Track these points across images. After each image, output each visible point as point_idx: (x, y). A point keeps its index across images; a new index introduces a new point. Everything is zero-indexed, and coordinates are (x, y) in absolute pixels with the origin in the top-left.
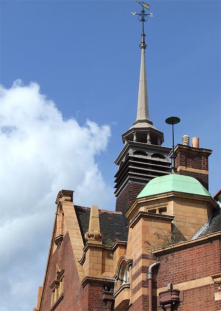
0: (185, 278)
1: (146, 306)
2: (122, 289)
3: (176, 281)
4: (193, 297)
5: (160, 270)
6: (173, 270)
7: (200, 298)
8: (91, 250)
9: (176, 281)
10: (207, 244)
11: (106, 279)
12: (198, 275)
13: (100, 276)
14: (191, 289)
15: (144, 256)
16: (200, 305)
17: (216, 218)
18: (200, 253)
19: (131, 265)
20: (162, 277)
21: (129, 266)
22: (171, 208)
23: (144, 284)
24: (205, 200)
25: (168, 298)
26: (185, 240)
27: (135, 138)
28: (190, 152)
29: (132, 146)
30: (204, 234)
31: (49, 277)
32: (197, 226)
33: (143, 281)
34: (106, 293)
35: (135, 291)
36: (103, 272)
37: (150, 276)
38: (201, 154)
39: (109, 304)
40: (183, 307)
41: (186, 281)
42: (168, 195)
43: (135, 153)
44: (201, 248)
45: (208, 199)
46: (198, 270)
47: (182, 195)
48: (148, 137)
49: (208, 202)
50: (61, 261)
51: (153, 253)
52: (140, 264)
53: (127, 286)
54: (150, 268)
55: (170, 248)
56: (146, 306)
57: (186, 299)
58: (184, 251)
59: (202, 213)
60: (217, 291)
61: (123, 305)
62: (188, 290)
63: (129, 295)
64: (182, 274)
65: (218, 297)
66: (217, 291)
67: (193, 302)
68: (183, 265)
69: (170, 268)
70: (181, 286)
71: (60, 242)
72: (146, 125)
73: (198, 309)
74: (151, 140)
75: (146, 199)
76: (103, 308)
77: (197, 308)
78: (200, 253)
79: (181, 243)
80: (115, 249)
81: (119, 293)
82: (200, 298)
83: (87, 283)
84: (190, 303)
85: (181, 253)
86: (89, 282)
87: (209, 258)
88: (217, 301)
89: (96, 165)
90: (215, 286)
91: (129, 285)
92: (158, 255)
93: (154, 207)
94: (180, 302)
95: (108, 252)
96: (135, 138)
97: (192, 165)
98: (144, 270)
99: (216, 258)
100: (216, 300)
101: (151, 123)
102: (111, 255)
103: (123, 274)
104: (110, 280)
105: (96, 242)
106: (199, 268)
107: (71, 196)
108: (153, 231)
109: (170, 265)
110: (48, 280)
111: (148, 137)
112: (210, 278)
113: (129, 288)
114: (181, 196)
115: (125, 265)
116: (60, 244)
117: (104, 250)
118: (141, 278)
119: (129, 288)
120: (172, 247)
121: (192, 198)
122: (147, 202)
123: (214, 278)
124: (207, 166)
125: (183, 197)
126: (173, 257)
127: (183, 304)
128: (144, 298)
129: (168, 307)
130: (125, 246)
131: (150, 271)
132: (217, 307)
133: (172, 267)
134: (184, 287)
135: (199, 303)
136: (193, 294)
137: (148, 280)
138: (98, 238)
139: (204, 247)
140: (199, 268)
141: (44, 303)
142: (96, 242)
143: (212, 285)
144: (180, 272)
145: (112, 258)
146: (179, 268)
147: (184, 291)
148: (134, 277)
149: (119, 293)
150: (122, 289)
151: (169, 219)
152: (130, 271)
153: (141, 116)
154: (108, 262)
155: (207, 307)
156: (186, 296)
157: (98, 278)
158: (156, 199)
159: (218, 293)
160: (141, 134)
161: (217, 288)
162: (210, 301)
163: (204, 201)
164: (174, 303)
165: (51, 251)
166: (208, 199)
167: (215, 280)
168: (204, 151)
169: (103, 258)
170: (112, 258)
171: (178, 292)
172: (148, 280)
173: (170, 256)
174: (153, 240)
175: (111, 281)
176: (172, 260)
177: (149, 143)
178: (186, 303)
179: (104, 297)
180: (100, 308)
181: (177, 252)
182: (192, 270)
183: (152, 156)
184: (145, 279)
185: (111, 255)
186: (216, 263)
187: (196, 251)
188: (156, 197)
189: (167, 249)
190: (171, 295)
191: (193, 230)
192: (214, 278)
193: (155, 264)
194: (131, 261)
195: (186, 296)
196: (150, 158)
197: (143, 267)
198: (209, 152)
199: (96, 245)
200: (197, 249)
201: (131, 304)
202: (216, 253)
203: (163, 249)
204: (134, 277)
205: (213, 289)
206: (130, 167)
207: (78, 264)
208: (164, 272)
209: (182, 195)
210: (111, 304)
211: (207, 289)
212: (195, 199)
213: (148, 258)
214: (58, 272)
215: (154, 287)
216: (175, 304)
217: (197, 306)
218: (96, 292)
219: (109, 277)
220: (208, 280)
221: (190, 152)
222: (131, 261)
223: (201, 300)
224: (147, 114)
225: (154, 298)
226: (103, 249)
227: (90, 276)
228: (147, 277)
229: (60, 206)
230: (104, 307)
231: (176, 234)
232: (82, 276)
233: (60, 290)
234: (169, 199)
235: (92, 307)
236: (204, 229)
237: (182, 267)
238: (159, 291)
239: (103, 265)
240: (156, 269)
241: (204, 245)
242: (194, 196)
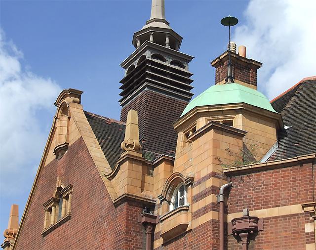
0: (266, 204)
1: (216, 233)
2: (178, 212)
3: (254, 206)
4: (276, 226)
5: (232, 192)
6: (249, 194)
7: (286, 228)
8: (130, 162)
9: (254, 206)
10: (296, 167)
11: (146, 199)
12: (283, 202)
13: (138, 194)
14: (274, 218)
15: (214, 175)
16: (286, 237)
17: (284, 140)
18: (286, 176)
19: (191, 184)
20: (235, 201)
21: (189, 185)
22: (239, 122)
23: (214, 207)
24: (275, 118)
25: (246, 225)
26: (253, 159)
27: (151, 39)
28: (239, 62)
29: (150, 47)
30: (272, 158)
31: (38, 193)
32: (267, 147)
33: (213, 203)
34: (147, 216)
35: (196, 215)
36: (142, 190)
37: (221, 199)
38: (249, 66)
39: (149, 228)
40: (262, 237)
41: (267, 208)
42: (236, 107)
43: (153, 57)
44: (287, 170)
45: (278, 117)
46: (283, 196)
47: (251, 109)
48: (167, 40)
49: (278, 120)
50: (66, 174)
51: (224, 171)
52: (210, 183)
53: (185, 208)
54: (222, 189)
55: (247, 168)
56: (216, 233)
57: (266, 228)
58: (265, 172)
59: (271, 132)
60: (308, 222)
61: (176, 231)
62: (270, 218)
63: (187, 219)
64: (262, 200)
65: (309, 228)
66: (308, 221)
67: (276, 233)
68: (263, 188)
69: (246, 191)
70: (261, 213)
71: (63, 151)
72: (164, 26)
73: (283, 240)
74: (170, 44)
75: (208, 109)
76: (142, 233)
77: (281, 239)
78: (286, 176)
79: (252, 165)
80: (157, 164)
81: (169, 217)
82: (286, 228)
83: (125, 201)
84: (272, 233)
85: (261, 174)
86: (128, 200)
87: (298, 183)
88: (308, 233)
89: (30, 74)
90: (306, 216)
91: (188, 207)
92: (229, 175)
93: (217, 119)
94: (258, 231)
95: (149, 167)
96: (151, 39)
97: (240, 78)
98: (214, 190)
99: (308, 184)
100: (307, 231)
101: (168, 24)
102: (151, 171)
103: (171, 194)
104: (151, 200)
105: (136, 154)
106: (284, 194)
107: (79, 97)
108: (224, 146)
109: (245, 188)
110: (36, 196)
111: (167, 40)
112: (300, 206)
113: (187, 210)
114: (251, 110)
115: (178, 184)
116: (63, 154)
117: (144, 165)
118: (210, 199)
119: (187, 210)
120: (250, 167)
121: (262, 114)
122: (209, 111)
123: (304, 207)
124: (256, 80)
125: (253, 111)
126: (250, 179)
127: (262, 234)
128: (214, 223)
129: (244, 236)
130: (171, 162)
131: (221, 191)
132: (308, 240)
133: (248, 190)
134: (263, 214)
135: (284, 234)
136: (277, 224)
137: (219, 203)
138: (138, 149)
139: (291, 170)
140: (284, 194)
141: (26, 224)
142: (136, 154)
143: (301, 214)
144: (259, 197)
145: (151, 174)
146: (257, 192)
147: (265, 219)
148: (196, 199)
149: (169, 217)
150: (178, 212)
151: (239, 134)
152: (189, 191)
153: (156, 13)
154: (148, 178)
155: (294, 239)
156: (267, 225)
157: (137, 197)
158: (221, 109)
159: (309, 224)
160: (160, 35)
161: (308, 219)
162: (298, 233)
163: (273, 119)
164: (252, 232)
165: (43, 161)
166: (278, 117)
167: (306, 209)
168: (253, 63)
169: (143, 174)
170: (152, 174)
171: (256, 219)
172: (219, 203)
173: (245, 177)
174: (224, 156)
175: (151, 202)
176: (248, 182)
177: (167, 47)
178: (266, 234)
179: (144, 219)
180: (139, 232)
181: (256, 174)
182: (275, 195)
183: (172, 63)
184: (215, 202)
185: (151, 171)
186: (307, 190)
187: (281, 174)
188: (222, 108)
189: (243, 168)
190: (250, 222)
191: (262, 151)
192: (304, 207)
193: (227, 185)
194: (192, 179)
195: (267, 225)
196: (169, 65)
197: (213, 187)
198: (258, 64)
199: (136, 157)
200: (282, 171)
201: (191, 230)
202: (308, 178)
203: (238, 168)
204: (196, 199)
205: (302, 219)
206: (147, 72)
207: (105, 179)
208: (237, 195)
209: (251, 109)
210: (152, 228)
211: (295, 218)
212: (264, 115)
213: (218, 178)
214: (60, 188)
215: (226, 212)
216: (252, 233)
217: (280, 238)
218: (134, 213)
219: (149, 197)
220: (296, 209)
221: (239, 62)
222: (192, 179)
223: (286, 231)
224: (163, 14)
225: (225, 224)
226: (144, 163)
227: (129, 193)
228: (218, 199)
229: (64, 109)
230: (143, 231)
231: (247, 154)
232: (113, 192)
233: (66, 207)
234: (237, 111)
235: (129, 230)
236: (274, 150)
237: (261, 191)
238: (230, 217)
239: (143, 182)
240: (227, 190)
241: (291, 168)
242: (265, 111)
